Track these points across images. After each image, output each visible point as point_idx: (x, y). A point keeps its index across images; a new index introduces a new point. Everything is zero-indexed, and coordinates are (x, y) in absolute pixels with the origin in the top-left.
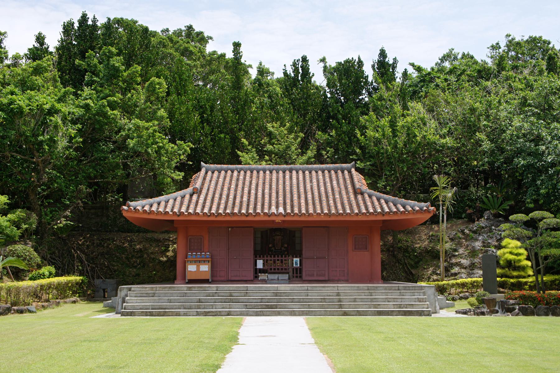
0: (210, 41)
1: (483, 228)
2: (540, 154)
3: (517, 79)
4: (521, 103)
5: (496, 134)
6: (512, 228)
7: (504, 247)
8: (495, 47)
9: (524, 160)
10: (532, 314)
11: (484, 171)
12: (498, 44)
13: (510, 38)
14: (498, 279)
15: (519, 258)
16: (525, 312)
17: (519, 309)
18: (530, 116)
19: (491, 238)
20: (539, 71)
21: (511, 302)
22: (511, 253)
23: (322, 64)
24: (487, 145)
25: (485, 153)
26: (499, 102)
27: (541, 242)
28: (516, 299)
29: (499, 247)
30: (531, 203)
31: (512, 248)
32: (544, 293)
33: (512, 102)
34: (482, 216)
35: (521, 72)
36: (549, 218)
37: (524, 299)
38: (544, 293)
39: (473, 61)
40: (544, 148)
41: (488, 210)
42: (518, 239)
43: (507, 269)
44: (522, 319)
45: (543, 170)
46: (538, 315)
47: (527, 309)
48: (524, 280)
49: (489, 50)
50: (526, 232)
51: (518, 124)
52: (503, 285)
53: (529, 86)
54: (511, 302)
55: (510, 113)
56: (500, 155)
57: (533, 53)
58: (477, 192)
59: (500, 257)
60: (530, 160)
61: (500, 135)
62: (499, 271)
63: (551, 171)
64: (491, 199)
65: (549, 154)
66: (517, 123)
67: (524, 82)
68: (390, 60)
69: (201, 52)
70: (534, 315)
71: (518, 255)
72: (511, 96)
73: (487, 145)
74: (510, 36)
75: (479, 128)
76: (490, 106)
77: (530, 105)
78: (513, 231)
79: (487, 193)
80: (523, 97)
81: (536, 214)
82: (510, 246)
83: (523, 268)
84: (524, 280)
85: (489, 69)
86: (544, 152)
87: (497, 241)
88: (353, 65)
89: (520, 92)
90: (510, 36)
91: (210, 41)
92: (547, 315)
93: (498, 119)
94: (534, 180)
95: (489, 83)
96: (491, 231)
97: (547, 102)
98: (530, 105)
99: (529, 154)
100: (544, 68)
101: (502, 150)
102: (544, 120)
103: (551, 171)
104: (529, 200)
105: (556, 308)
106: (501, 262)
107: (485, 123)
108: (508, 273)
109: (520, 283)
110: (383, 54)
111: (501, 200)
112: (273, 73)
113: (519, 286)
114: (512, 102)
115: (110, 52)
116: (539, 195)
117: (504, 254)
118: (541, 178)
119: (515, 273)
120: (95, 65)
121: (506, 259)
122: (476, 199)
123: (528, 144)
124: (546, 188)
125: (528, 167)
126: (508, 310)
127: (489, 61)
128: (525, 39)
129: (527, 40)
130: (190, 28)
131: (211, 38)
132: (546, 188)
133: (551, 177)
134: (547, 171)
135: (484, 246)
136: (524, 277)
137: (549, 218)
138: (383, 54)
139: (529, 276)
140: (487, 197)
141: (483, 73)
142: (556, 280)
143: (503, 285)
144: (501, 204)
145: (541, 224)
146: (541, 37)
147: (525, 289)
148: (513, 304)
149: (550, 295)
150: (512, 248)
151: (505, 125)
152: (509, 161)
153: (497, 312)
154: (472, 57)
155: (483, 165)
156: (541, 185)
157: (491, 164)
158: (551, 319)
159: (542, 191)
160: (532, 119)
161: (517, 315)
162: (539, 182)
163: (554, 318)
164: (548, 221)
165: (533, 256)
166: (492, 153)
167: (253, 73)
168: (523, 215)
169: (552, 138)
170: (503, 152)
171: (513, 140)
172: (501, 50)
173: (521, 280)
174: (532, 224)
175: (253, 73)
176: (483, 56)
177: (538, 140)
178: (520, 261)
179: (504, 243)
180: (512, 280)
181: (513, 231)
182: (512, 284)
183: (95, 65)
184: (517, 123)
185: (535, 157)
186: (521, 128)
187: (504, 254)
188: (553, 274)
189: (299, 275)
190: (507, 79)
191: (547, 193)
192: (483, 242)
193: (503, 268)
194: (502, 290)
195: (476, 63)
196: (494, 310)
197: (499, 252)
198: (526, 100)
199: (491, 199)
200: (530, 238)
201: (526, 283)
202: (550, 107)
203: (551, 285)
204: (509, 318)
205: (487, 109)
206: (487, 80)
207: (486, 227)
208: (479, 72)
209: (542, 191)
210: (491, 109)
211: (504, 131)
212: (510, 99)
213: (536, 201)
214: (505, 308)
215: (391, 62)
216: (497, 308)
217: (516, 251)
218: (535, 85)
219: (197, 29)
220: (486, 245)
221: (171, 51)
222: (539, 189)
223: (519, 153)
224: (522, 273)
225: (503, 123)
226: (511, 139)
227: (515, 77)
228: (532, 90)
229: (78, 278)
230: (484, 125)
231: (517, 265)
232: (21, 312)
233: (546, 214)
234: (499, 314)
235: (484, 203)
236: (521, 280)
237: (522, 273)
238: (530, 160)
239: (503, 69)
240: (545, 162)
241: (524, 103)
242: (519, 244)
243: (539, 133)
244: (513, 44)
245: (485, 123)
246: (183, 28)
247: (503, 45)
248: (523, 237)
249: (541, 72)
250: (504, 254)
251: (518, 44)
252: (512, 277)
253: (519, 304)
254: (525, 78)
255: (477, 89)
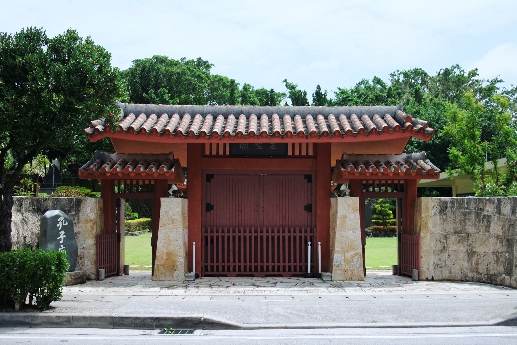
0: (212, 67)
10: (378, 236)
23: (285, 84)
48: (387, 221)
68: (323, 91)
69: (208, 76)
83: (388, 215)
88: (300, 96)
91: (212, 67)
92: (385, 237)
110: (318, 88)
112: (253, 87)
115: (164, 91)
120: (154, 98)
130: (200, 59)
131: (213, 65)
138: (318, 88)
139: (391, 219)
158: (387, 238)
167: (240, 88)
175: (240, 88)
183: (154, 98)
189: (209, 235)
193: (377, 214)
201: (388, 222)
215: (323, 93)
219: (204, 59)
221: (190, 77)
229: (149, 219)
232: (132, 235)
246: (196, 60)
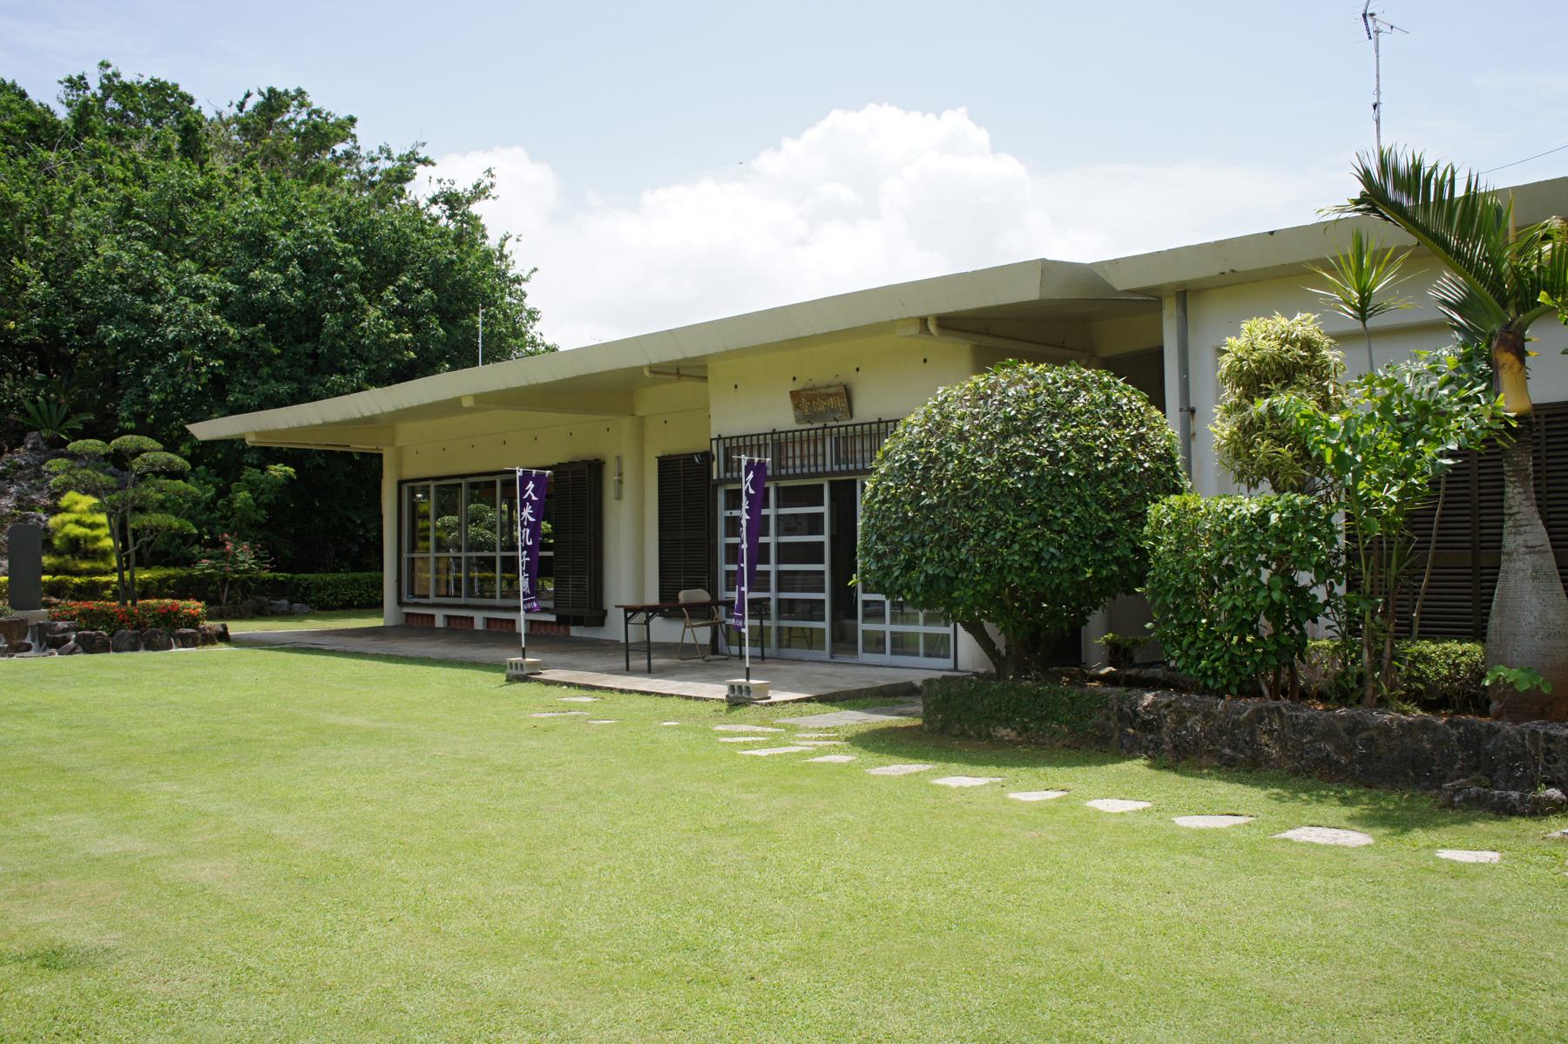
1: (20, 467)
2: (152, 321)
3: (118, 161)
4: (120, 210)
5: (60, 268)
6: (72, 468)
7: (66, 510)
8: (77, 84)
9: (118, 328)
10: (105, 648)
11: (33, 346)
12: (82, 78)
13: (109, 71)
14: (45, 578)
15: (96, 533)
16: (90, 646)
17: (76, 641)
18: (136, 238)
19: (39, 490)
20: (163, 151)
21: (61, 624)
22: (78, 523)
24: (38, 289)
25: (33, 305)
26: (72, 199)
27: (133, 499)
28: (72, 618)
29: (54, 510)
30: (129, 420)
31: (80, 513)
32: (134, 604)
33: (102, 204)
34: (20, 443)
35: (128, 147)
36: (152, 450)
37: (91, 618)
38: (134, 604)
39: (23, 103)
40: (159, 309)
41: (32, 429)
42: (95, 494)
43: (68, 557)
44: (82, 660)
45: (157, 354)
46: (116, 650)
47: (93, 639)
48: (104, 579)
49: (61, 87)
50: (103, 477)
51: (109, 253)
52: (56, 590)
53: (141, 177)
54: (61, 624)
55: (94, 226)
56: (68, 314)
57: (159, 113)
58: (13, 389)
59: (55, 531)
60: (132, 330)
61: (68, 273)
62: (46, 560)
63: (173, 358)
64: (44, 407)
65: (169, 323)
66: (106, 249)
67: (131, 166)
70: (107, 650)
71: (93, 526)
72: (103, 191)
73: (38, 289)
74: (108, 66)
75: (23, 248)
76: (49, 205)
77: (138, 217)
78: (74, 476)
79: (36, 393)
80: (125, 197)
81: (127, 441)
82: (78, 508)
83: (103, 555)
84: (104, 579)
85: (57, 125)
86: (160, 317)
87: (51, 497)
89: (120, 185)
90: (108, 66)
92: (135, 648)
93: (68, 236)
94: (139, 374)
95: (52, 155)
96: (38, 474)
97: (172, 215)
98: (138, 217)
99: (131, 319)
100: (175, 147)
101: (76, 304)
102: (165, 252)
103: (173, 358)
104: (125, 414)
105: (154, 634)
106: (56, 542)
107: (36, 239)
108: (71, 565)
109: (95, 584)
111: (65, 409)
113: (93, 591)
114: (102, 204)
116: (148, 404)
117: (65, 525)
118: (154, 371)
119: (85, 565)
121: (67, 535)
122: (11, 406)
123: (129, 297)
124: (162, 390)
125: (128, 345)
126: (52, 642)
127: (62, 114)
128: (145, 80)
129: (147, 85)
132: (162, 390)
133: (171, 371)
134: (165, 354)
135: (20, 508)
136: (105, 573)
137: (152, 450)
140: (35, 402)
141: (40, 129)
142: (170, 577)
143: (56, 590)
144: (67, 417)
145: (137, 464)
146: (176, 86)
147: (103, 598)
148: (64, 630)
149: (147, 608)
150: (80, 513)
151: (82, 252)
152: (86, 329)
153: (28, 648)
154: (23, 95)
155: (27, 331)
156: (152, 383)
157: (49, 331)
159: (154, 397)
160: (140, 245)
161: (72, 652)
162: (148, 379)
163: (88, 656)
164: (150, 456)
165: (120, 532)
166: (51, 308)
168: (99, 442)
169: (180, 291)
170: (76, 309)
171: (97, 284)
172: (88, 93)
173: (97, 578)
174: (119, 460)
176: (48, 95)
177: (149, 291)
178: (97, 539)
179: (64, 502)
180: (77, 580)
181: (74, 476)
182: (78, 587)
184: (106, 249)
185: (143, 327)
186: (112, 262)
187: (64, 524)
188: (167, 565)
190: (95, 153)
191: (164, 402)
192: (19, 499)
193: (59, 554)
194: (54, 600)
195: (29, 107)
196: (21, 644)
197: (53, 521)
198: (131, 205)
199: (44, 407)
200: (113, 491)
201: (107, 585)
202: (181, 229)
203: (160, 588)
204: (55, 660)
205: (42, 211)
206: (51, 149)
207: (29, 465)
208: (32, 126)
209: (154, 397)
210: (53, 212)
211: (79, 264)
212: (99, 198)
213: (140, 417)
214: (47, 639)
216: (28, 640)
217: (89, 519)
218: (154, 177)
220: (24, 503)
222: (147, 392)
223: (110, 313)
224: (101, 565)
225: (78, 247)
226: (93, 283)
227: (112, 154)
228: (145, 187)
230: (35, 244)
231: (90, 547)
233: (148, 442)
234: (32, 653)
235: (28, 415)
236: (97, 578)
237: (101, 565)
238: (132, 330)
239: (89, 132)
240: (162, 337)
241: (126, 209)
242: (91, 500)
243: (152, 276)
244: (114, 86)
245: (36, 239)
247: (94, 85)
248: (1104, 593)
249: (166, 154)
250: (64, 524)
251: (127, 88)
252: (78, 574)
253: (77, 629)
254: (134, 160)
255: (23, 162)
